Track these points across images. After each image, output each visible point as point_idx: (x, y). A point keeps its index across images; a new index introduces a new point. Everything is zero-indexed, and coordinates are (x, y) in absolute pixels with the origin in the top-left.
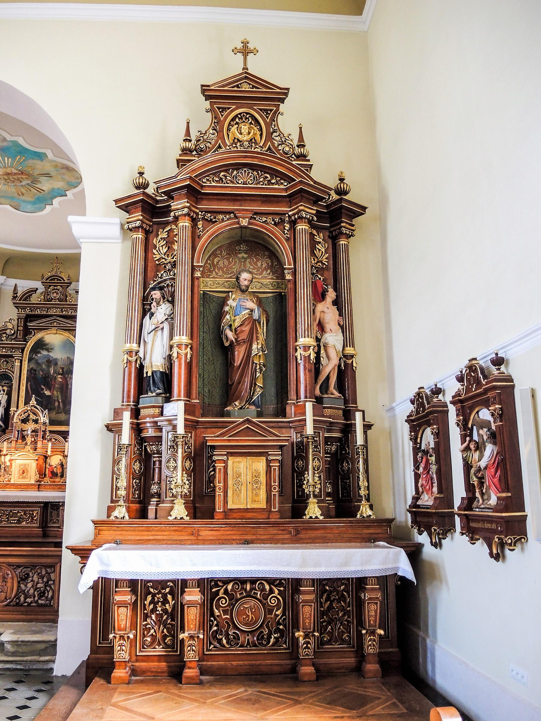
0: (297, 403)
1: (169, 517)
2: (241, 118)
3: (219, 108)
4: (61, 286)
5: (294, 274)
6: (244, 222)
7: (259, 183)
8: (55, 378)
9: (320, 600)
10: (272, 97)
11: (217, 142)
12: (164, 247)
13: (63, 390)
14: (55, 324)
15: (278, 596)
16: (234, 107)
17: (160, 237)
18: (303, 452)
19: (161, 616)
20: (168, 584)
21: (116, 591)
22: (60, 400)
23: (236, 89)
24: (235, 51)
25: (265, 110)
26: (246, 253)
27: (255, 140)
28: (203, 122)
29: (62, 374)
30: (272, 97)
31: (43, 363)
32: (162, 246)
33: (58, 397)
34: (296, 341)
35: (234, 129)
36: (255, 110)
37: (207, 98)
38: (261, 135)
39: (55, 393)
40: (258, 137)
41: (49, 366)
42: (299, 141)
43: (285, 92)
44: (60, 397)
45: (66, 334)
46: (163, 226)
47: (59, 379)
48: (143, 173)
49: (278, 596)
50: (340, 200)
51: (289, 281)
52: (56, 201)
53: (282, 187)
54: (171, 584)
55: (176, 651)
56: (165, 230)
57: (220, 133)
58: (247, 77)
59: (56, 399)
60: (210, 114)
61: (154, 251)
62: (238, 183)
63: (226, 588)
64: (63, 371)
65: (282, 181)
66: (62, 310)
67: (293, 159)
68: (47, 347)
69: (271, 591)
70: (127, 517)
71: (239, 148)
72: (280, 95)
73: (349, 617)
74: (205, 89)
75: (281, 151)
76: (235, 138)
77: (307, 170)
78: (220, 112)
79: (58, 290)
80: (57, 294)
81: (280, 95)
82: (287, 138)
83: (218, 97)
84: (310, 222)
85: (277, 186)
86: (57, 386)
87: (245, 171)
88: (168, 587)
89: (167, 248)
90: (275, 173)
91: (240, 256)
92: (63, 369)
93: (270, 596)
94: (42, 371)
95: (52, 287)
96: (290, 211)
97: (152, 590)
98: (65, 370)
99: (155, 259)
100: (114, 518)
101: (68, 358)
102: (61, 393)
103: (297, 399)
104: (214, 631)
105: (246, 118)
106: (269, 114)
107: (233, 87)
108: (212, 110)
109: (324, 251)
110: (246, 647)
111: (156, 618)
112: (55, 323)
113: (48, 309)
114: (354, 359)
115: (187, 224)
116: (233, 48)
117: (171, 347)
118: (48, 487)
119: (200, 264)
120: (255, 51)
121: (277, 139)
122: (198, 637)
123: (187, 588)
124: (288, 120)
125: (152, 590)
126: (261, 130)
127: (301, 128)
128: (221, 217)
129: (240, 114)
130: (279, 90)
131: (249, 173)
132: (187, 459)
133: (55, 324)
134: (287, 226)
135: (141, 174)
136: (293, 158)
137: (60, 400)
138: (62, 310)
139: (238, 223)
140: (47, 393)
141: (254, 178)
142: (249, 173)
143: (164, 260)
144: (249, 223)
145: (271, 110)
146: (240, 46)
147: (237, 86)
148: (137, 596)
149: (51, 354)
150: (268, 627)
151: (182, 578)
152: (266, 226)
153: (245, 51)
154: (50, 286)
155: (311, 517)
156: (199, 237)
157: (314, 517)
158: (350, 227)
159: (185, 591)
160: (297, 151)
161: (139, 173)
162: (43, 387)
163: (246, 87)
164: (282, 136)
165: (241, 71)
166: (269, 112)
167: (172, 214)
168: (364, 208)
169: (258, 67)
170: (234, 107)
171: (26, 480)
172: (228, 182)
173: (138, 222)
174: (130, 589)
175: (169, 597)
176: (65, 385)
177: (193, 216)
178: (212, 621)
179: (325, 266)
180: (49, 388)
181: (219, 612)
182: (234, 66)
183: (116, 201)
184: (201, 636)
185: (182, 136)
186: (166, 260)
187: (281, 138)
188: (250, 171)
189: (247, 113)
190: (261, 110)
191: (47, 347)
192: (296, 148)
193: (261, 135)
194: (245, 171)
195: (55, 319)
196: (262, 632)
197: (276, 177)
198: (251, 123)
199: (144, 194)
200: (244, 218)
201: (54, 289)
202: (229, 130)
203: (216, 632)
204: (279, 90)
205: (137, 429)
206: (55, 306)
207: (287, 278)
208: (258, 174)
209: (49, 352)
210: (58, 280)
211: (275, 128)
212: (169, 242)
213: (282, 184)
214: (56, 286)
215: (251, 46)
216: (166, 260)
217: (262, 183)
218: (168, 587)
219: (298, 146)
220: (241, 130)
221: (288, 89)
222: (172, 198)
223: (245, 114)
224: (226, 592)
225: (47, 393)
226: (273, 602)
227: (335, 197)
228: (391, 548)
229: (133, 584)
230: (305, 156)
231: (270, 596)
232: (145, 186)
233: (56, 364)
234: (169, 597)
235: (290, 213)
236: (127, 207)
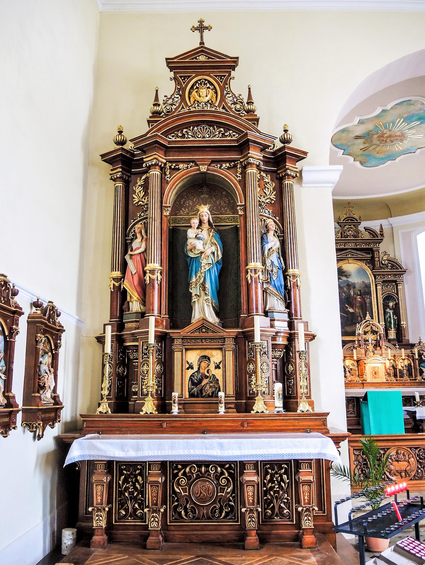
0: (249, 316)
1: (141, 413)
2: (201, 84)
3: (181, 77)
4: (354, 225)
5: (245, 210)
6: (203, 169)
7: (215, 136)
8: (356, 299)
9: (119, 482)
10: (222, 66)
11: (180, 103)
12: (142, 191)
13: (363, 307)
14: (350, 256)
15: (228, 477)
16: (194, 75)
17: (139, 184)
18: (253, 357)
19: (132, 493)
20: (283, 466)
21: (149, 473)
22: (362, 316)
23: (195, 60)
24: (194, 29)
25: (219, 76)
26: (207, 194)
27: (212, 102)
28: (168, 88)
29: (360, 295)
30: (222, 66)
31: (344, 287)
32: (140, 191)
33: (360, 313)
34: (247, 265)
35: (194, 93)
36: (211, 77)
37: (171, 69)
38: (217, 97)
39: (357, 310)
40: (214, 100)
41: (349, 289)
42: (248, 99)
43: (235, 61)
44: (361, 313)
45: (359, 264)
46: (140, 175)
47: (359, 299)
48: (122, 132)
49: (228, 477)
50: (284, 147)
51: (241, 215)
52: (398, 160)
53: (234, 138)
54: (286, 466)
55: (146, 523)
56: (142, 179)
57: (182, 97)
58: (202, 49)
59: (358, 315)
60: (173, 81)
61: (134, 196)
62: (198, 137)
63: (185, 472)
64: (361, 293)
65: (234, 133)
66: (356, 244)
67: (243, 115)
68: (345, 274)
69: (222, 473)
70: (110, 412)
71: (197, 108)
72: (232, 64)
73: (142, 497)
74: (169, 62)
75: (234, 109)
76: (195, 100)
77: (254, 124)
78: (182, 80)
79: (352, 228)
80: (352, 231)
81: (232, 64)
82: (238, 98)
83: (182, 67)
84: (258, 166)
85: (230, 138)
86: (357, 304)
87: (203, 128)
88: (138, 469)
89: (144, 193)
90: (227, 127)
91: (202, 196)
92: (360, 291)
93: (222, 477)
94: (345, 293)
95: (347, 226)
96: (241, 158)
97: (125, 472)
98: (362, 291)
99: (135, 202)
100: (99, 413)
101: (363, 282)
102: (362, 309)
103: (249, 314)
104: (175, 505)
105: (205, 84)
106: (223, 79)
107: (193, 59)
108: (175, 79)
109: (272, 190)
110: (202, 519)
111: (129, 494)
112: (350, 255)
113: (345, 244)
114: (298, 278)
115: (157, 173)
116: (191, 27)
117: (145, 273)
118: (395, 385)
119: (168, 205)
120: (208, 28)
121: (229, 100)
122: (257, 510)
123: (245, 470)
124: (238, 84)
125: (125, 472)
126: (216, 93)
127: (157, 91)
128: (181, 166)
129: (200, 80)
130: (229, 60)
131: (206, 128)
132: (158, 363)
133: (350, 256)
134: (240, 170)
135: (120, 132)
136: (243, 113)
137: (362, 316)
138: (356, 244)
139: (199, 170)
140: (351, 310)
141: (211, 133)
142: (206, 128)
143: (140, 203)
144: (208, 170)
145: (224, 76)
146: (205, 24)
147: (196, 58)
148: (113, 477)
149: (350, 280)
150: (219, 502)
151: (240, 460)
152: (223, 172)
153: (201, 28)
154: (345, 225)
155: (146, 413)
156: (168, 182)
157: (149, 413)
158: (295, 170)
159: (244, 473)
160: (247, 107)
161: (118, 132)
162: (346, 305)
163: (202, 58)
164: (234, 97)
165: (198, 45)
166: (223, 77)
167: (144, 165)
168: (305, 153)
169: (212, 42)
170: (194, 75)
171: (379, 379)
172: (190, 137)
173: (119, 173)
174: (160, 472)
175: (285, 477)
176: (364, 304)
177: (161, 165)
178: (173, 497)
179: (273, 202)
180: (352, 307)
181: (179, 490)
182: (192, 42)
183: (102, 156)
184: (260, 510)
185: (152, 101)
186: (143, 202)
187: (233, 98)
188: (207, 127)
189: (206, 80)
190: (216, 76)
191: (345, 274)
192: (246, 105)
193: (217, 97)
194: (203, 128)
195: (350, 252)
196: (216, 507)
197: (230, 130)
198: (209, 88)
199: (123, 149)
200: (203, 165)
201: (349, 228)
202: (190, 93)
203: (177, 507)
204: (229, 60)
205: (119, 340)
206: (350, 241)
207: (240, 213)
208: (214, 129)
209: (347, 278)
210: (351, 220)
211: (228, 90)
212: (146, 187)
213: (234, 135)
214: (350, 225)
215: (197, 25)
216: (143, 202)
217: (217, 136)
218: (138, 469)
219: (248, 103)
220: (199, 94)
221: (237, 58)
222: (144, 152)
223: (204, 80)
224: (184, 474)
225: (351, 310)
226: (223, 482)
227: (279, 145)
228: (324, 437)
229: (256, 464)
230: (253, 111)
231: (222, 477)
232: (123, 143)
233: (354, 287)
234: (285, 477)
235: (241, 160)
236: (110, 160)
